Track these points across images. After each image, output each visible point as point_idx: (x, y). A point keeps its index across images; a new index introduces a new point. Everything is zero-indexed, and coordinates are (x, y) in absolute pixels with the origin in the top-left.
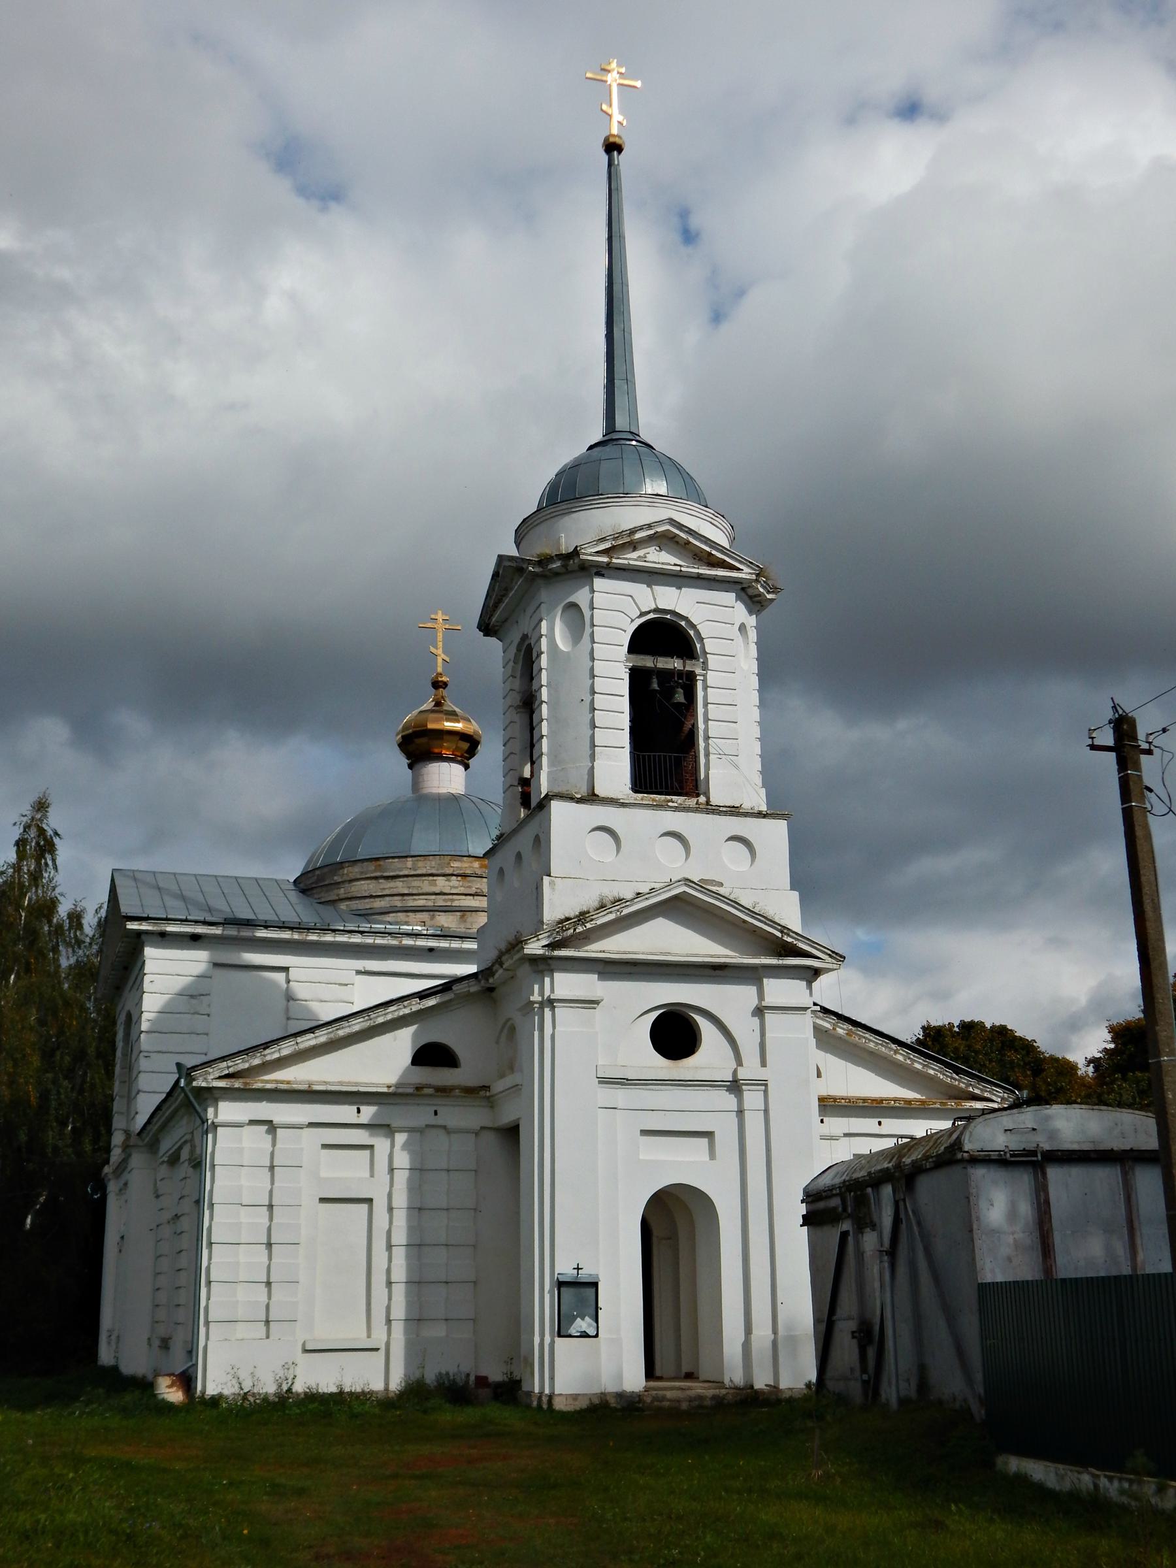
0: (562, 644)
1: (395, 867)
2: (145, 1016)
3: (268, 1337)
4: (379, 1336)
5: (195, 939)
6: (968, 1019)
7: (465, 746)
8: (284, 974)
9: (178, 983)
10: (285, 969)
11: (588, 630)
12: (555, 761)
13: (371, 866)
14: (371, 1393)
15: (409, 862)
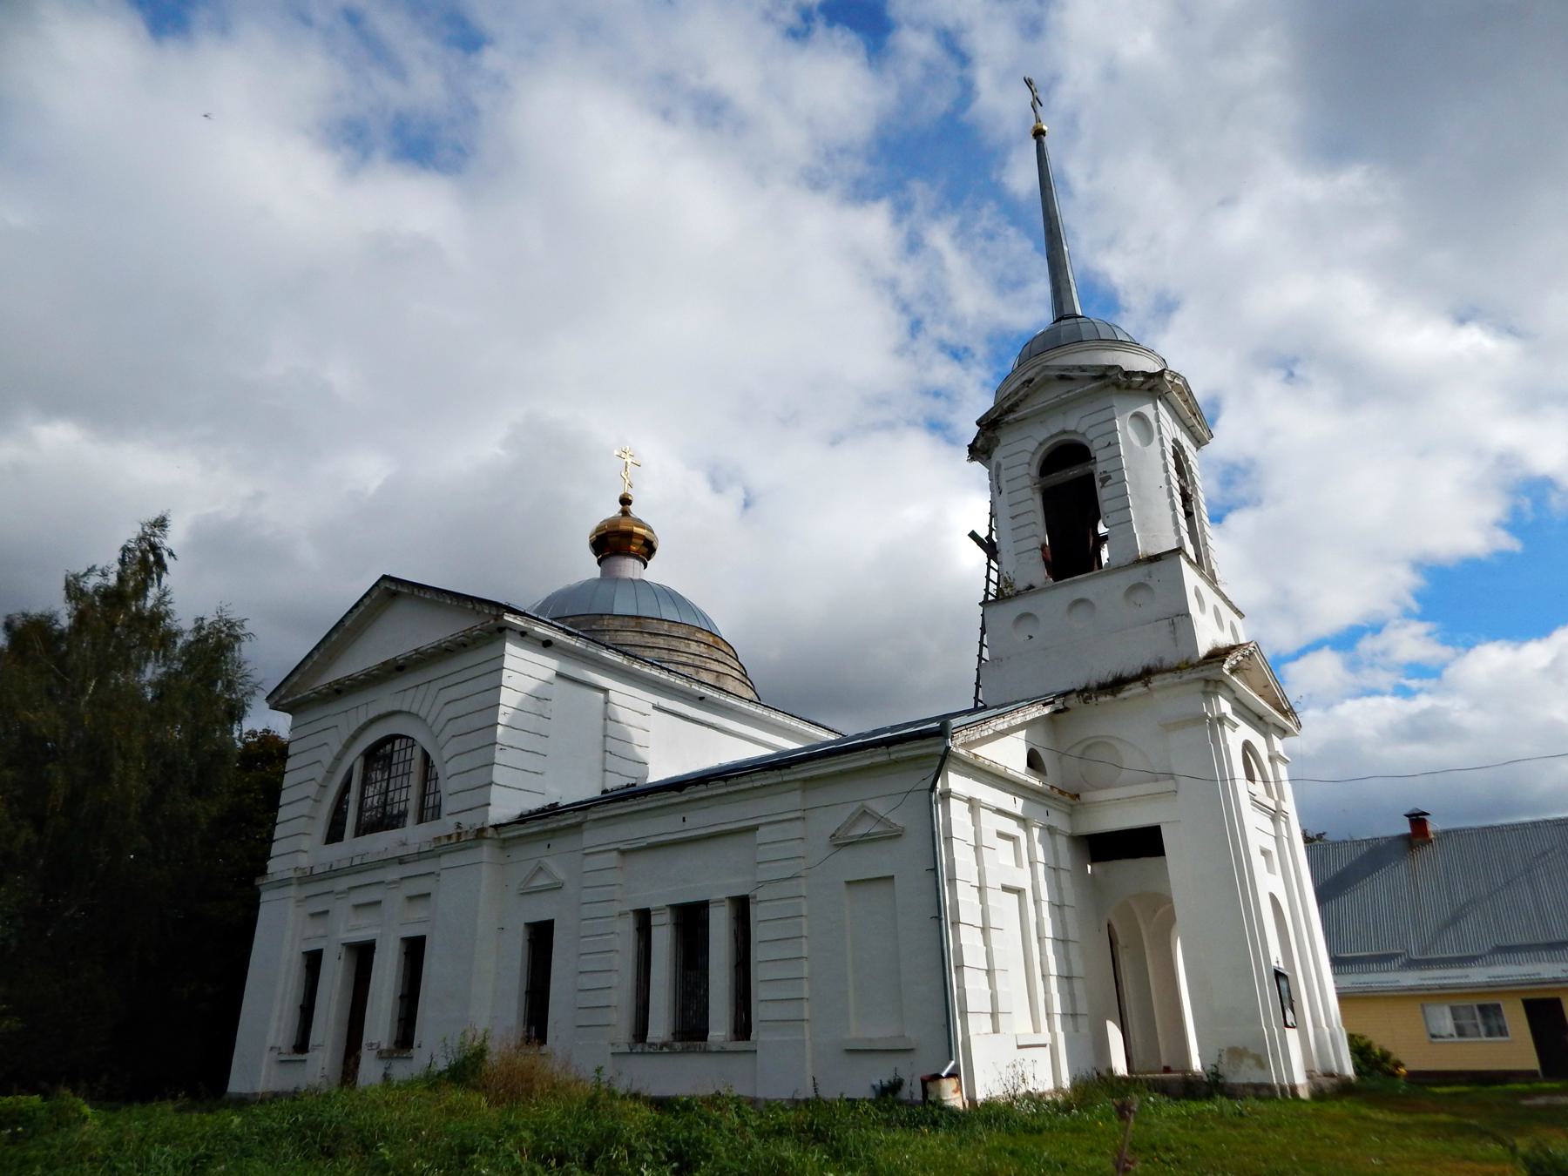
0: (1136, 442)
1: (654, 626)
2: (502, 709)
3: (1019, 1047)
4: (1045, 1037)
5: (547, 644)
6: (336, 844)
7: (645, 550)
8: (602, 695)
9: (531, 685)
10: (605, 691)
11: (1156, 437)
12: (1143, 527)
13: (633, 623)
14: (1034, 1098)
15: (666, 626)
